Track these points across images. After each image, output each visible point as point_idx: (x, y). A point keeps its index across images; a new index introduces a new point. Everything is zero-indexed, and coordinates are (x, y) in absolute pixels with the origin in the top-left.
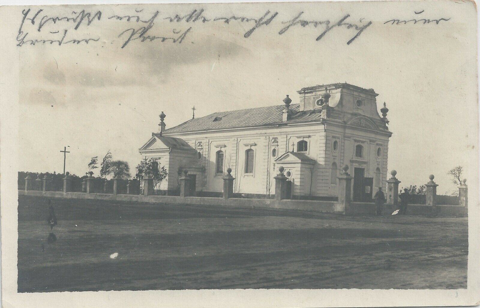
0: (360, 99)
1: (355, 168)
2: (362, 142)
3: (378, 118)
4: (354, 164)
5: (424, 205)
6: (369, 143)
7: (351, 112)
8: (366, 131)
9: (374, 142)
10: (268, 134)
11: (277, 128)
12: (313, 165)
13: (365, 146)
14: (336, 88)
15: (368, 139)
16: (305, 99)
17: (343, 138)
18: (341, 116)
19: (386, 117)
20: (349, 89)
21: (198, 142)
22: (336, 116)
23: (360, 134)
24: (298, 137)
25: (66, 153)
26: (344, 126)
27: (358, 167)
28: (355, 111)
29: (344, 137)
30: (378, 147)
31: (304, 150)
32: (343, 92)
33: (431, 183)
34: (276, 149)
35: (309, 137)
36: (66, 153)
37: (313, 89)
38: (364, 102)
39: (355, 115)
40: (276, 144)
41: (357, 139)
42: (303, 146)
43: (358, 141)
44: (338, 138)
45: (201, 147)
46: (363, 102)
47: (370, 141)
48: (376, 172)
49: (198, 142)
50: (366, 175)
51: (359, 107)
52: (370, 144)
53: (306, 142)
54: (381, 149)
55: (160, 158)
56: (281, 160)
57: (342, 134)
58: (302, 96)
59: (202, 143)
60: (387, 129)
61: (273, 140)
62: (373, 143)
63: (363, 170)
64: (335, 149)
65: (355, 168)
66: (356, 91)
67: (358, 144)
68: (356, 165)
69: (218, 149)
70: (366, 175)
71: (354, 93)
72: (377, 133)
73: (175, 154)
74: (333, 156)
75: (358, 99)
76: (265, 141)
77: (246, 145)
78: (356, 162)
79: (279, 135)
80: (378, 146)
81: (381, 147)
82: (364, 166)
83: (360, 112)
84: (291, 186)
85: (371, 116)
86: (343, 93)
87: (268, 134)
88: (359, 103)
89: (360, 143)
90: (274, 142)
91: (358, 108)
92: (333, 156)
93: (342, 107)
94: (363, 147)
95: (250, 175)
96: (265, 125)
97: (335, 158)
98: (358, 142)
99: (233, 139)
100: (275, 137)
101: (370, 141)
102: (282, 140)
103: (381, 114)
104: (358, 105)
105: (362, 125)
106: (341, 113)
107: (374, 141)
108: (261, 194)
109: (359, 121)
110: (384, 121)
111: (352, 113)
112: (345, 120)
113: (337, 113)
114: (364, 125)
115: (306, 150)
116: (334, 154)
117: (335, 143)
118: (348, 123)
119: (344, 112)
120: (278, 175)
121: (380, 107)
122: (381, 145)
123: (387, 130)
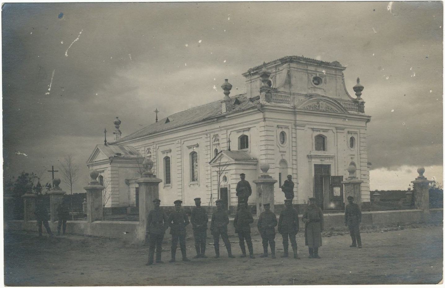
0: (318, 76)
1: (315, 165)
2: (324, 131)
3: (347, 98)
4: (313, 160)
5: (278, 221)
6: (335, 131)
7: (305, 93)
8: (330, 116)
9: (304, 126)
10: (209, 132)
11: (217, 122)
12: (255, 165)
13: (330, 137)
14: (283, 63)
15: (333, 127)
16: (251, 82)
17: (293, 127)
18: (289, 100)
19: (362, 97)
20: (298, 63)
21: (147, 149)
22: (281, 99)
23: (321, 122)
24: (238, 131)
25: (54, 172)
26: (294, 112)
27: (320, 163)
28: (310, 92)
29: (296, 125)
30: (350, 136)
31: (246, 147)
32: (290, 67)
33: (349, 179)
34: (217, 148)
35: (249, 129)
36: (52, 172)
37: (258, 69)
38: (324, 79)
39: (311, 96)
40: (217, 142)
41: (315, 127)
42: (244, 142)
43: (318, 130)
44: (287, 127)
45: (217, 142)
46: (323, 80)
47: (337, 128)
48: (279, 166)
49: (147, 149)
50: (333, 174)
51: (316, 86)
52: (337, 132)
53: (247, 137)
54: (356, 139)
55: (103, 171)
56: (215, 161)
57: (292, 122)
58: (249, 79)
59: (150, 149)
60: (362, 112)
61: (214, 139)
62: (303, 128)
63: (329, 166)
64: (283, 142)
65: (315, 165)
66: (311, 65)
67: (318, 133)
68: (318, 162)
69: (165, 155)
70: (333, 174)
71: (307, 67)
72: (345, 118)
73: (119, 165)
74: (280, 152)
75: (314, 76)
76: (206, 140)
77: (189, 147)
78: (316, 157)
79: (219, 131)
80: (350, 134)
81: (355, 137)
82: (326, 162)
83: (319, 92)
84: (227, 194)
85: (335, 97)
86: (291, 69)
87: (209, 132)
88: (318, 80)
89: (353, 134)
90: (215, 140)
91: (315, 87)
92: (280, 152)
93: (291, 87)
94: (326, 137)
95: (195, 184)
96: (204, 120)
97: (353, 157)
98: (317, 131)
99: (177, 142)
100: (216, 133)
101: (337, 128)
102: (223, 137)
103: (353, 95)
104: (316, 84)
105: (320, 109)
106: (289, 96)
107: (343, 129)
108: (207, 206)
109: (316, 105)
110: (359, 105)
111: (306, 94)
112: (296, 103)
113: (283, 95)
114: (324, 109)
115: (247, 147)
116: (282, 149)
117: (283, 134)
118: (299, 108)
119: (294, 94)
120: (416, 179)
121: (350, 85)
122: (356, 133)
123: (363, 114)
